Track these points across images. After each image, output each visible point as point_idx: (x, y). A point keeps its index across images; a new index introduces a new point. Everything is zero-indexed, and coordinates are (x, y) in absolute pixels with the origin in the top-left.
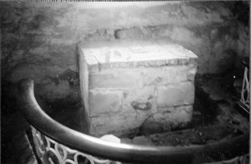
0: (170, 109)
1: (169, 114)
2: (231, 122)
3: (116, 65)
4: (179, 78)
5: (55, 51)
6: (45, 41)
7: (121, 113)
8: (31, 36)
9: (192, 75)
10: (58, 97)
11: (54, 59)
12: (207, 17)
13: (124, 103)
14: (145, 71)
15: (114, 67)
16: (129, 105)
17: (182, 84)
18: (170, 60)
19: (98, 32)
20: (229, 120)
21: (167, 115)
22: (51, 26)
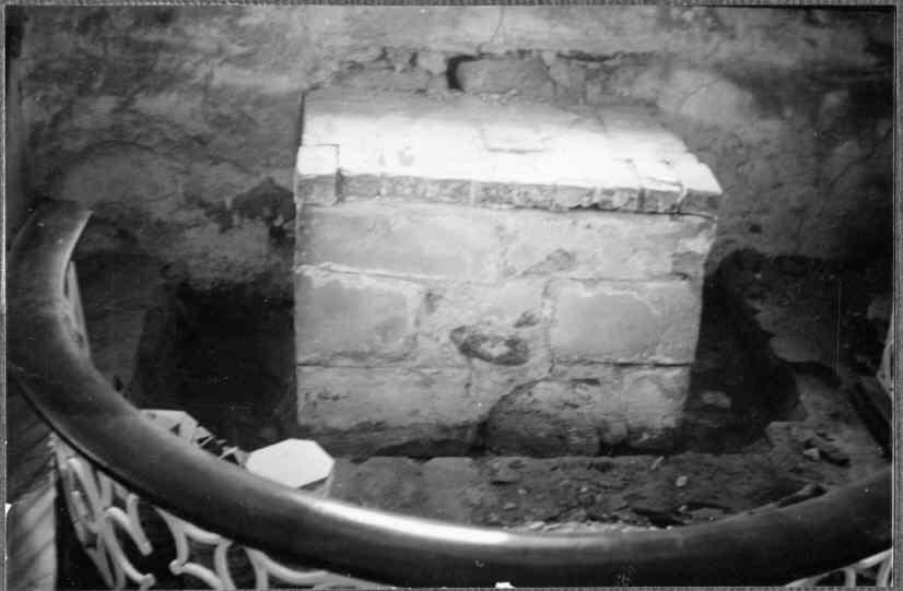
0: (596, 373)
1: (593, 390)
2: (814, 452)
3: (399, 188)
4: (639, 264)
5: (225, 110)
6: (193, 71)
7: (411, 364)
8: (145, 47)
9: (691, 256)
10: (228, 276)
11: (222, 138)
12: (812, 43)
13: (425, 328)
14: (511, 220)
15: (393, 193)
16: (445, 338)
17: (652, 285)
18: (610, 193)
19: (383, 56)
20: (808, 445)
21: (584, 393)
22: (216, 20)
